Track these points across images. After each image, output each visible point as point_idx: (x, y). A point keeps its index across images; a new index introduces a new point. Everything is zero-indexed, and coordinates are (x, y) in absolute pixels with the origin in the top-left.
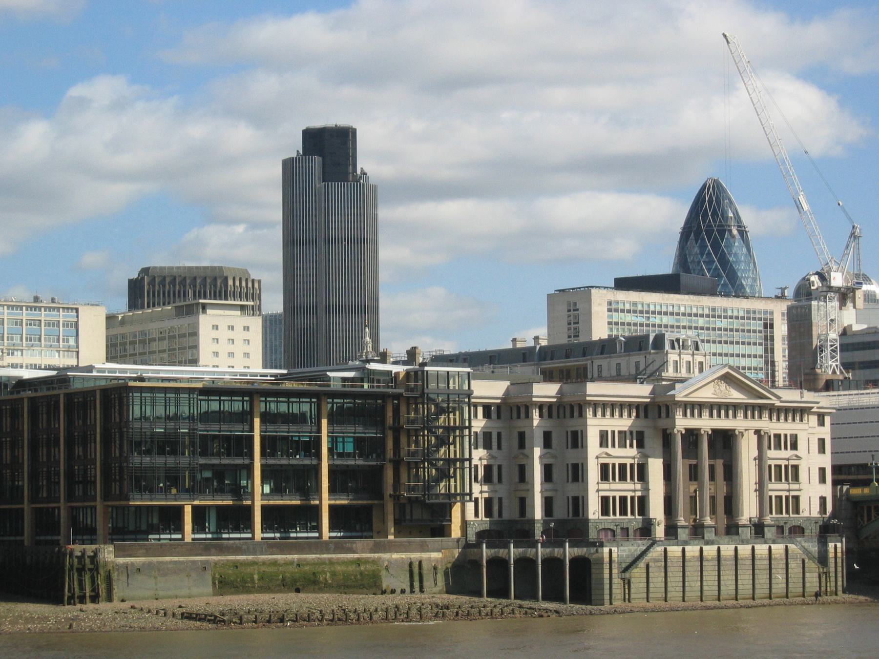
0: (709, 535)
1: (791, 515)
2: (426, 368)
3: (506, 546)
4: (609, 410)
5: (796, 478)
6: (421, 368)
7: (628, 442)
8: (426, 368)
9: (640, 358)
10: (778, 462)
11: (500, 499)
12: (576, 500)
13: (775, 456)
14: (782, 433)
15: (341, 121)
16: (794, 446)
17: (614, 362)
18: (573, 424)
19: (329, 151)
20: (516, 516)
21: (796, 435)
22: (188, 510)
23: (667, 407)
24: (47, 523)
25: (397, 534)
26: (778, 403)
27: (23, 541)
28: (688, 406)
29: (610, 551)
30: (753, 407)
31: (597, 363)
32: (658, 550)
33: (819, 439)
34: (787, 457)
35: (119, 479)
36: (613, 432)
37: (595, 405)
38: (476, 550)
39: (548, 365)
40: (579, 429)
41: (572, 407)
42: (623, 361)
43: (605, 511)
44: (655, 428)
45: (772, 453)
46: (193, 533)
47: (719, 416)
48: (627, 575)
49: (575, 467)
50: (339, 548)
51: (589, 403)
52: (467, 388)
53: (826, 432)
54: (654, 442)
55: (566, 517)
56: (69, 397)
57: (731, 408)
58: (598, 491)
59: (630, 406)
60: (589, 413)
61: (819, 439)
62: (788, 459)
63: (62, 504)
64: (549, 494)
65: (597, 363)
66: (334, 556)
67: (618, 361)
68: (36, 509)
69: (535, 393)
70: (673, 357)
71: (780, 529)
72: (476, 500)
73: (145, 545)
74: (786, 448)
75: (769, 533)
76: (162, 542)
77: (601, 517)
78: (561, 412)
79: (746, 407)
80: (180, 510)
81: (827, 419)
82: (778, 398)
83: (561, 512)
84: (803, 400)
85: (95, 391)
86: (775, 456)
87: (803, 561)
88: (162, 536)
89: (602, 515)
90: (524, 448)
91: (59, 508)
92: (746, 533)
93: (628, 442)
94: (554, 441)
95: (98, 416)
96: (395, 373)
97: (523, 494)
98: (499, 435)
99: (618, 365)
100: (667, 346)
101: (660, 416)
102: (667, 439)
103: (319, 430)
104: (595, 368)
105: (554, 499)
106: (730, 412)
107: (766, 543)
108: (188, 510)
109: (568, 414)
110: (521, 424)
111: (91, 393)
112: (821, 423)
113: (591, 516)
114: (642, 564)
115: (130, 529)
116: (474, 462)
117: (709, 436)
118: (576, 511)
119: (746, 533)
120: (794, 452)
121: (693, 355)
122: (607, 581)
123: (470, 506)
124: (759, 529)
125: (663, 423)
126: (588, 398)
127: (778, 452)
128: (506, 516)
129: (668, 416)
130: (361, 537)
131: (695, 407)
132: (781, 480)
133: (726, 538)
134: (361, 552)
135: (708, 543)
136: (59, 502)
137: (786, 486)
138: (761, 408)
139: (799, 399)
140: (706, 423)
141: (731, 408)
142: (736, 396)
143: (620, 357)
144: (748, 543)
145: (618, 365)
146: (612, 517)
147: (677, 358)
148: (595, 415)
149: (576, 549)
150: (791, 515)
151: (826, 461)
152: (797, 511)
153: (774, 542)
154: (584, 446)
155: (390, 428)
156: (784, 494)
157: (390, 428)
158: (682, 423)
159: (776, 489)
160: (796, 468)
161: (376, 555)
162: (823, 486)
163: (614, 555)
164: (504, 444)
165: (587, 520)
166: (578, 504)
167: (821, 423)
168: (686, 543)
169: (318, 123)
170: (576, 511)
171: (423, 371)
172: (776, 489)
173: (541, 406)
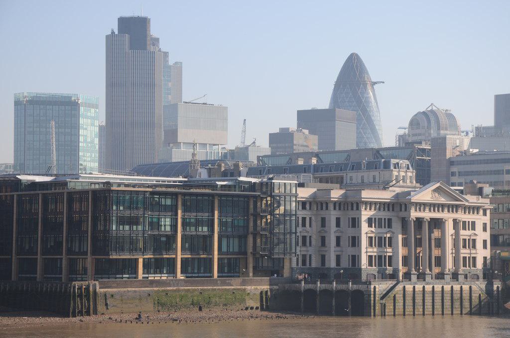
0: (428, 278)
1: (388, 267)
2: (273, 181)
3: (315, 283)
4: (368, 206)
5: (474, 247)
6: (270, 181)
7: (373, 224)
8: (273, 181)
9: (376, 173)
10: (464, 237)
11: (310, 255)
12: (354, 257)
13: (464, 234)
14: (467, 220)
15: (142, 14)
16: (474, 228)
17: (360, 174)
18: (352, 214)
19: (133, 33)
20: (319, 265)
21: (486, 223)
22: (141, 261)
23: (406, 205)
24: (52, 267)
25: (255, 275)
26: (467, 204)
27: (36, 277)
28: (450, 206)
29: (375, 287)
30: (453, 206)
31: (350, 175)
32: (400, 287)
33: (483, 223)
34: (469, 234)
35: (103, 243)
36: (469, 222)
37: (366, 203)
38: (297, 285)
39: (318, 175)
40: (356, 217)
41: (352, 204)
42: (365, 174)
43: (370, 264)
44: (398, 217)
45: (462, 232)
46: (143, 274)
47: (434, 211)
48: (384, 301)
49: (354, 238)
50: (224, 284)
51: (363, 202)
52: (283, 192)
53: (487, 219)
54: (397, 225)
55: (348, 267)
56: (71, 194)
57: (441, 207)
58: (367, 252)
59: (376, 203)
60: (363, 208)
61: (483, 223)
62: (470, 236)
63: (64, 256)
64: (338, 253)
65: (350, 175)
66: (220, 287)
67: (363, 174)
68: (70, 259)
69: (332, 196)
70: (395, 173)
71: (466, 277)
72: (298, 255)
73: (116, 281)
74: (469, 230)
75: (461, 278)
76: (124, 279)
77: (368, 267)
78: (346, 206)
79: (449, 206)
80: (136, 260)
81: (488, 212)
82: (467, 201)
83: (345, 263)
84: (479, 202)
85: (88, 191)
86: (464, 234)
87: (480, 295)
88: (124, 276)
89: (302, 265)
90: (325, 227)
91: (61, 259)
92: (448, 278)
93: (373, 224)
94: (342, 223)
95: (90, 206)
96: (254, 183)
97: (324, 253)
98: (310, 219)
99: (362, 177)
100: (392, 168)
101: (401, 210)
102: (404, 222)
103: (213, 215)
104: (349, 178)
105: (341, 256)
106: (422, 208)
107: (459, 284)
108: (141, 261)
109: (350, 208)
110: (323, 213)
111: (86, 192)
112: (485, 214)
113: (363, 267)
114: (391, 295)
115: (109, 269)
116: (298, 234)
117: (429, 223)
118: (354, 263)
119: (448, 278)
120: (473, 232)
121: (406, 172)
122: (372, 302)
123: (294, 259)
124: (455, 276)
125: (403, 214)
126: (363, 200)
127: (464, 231)
128: (314, 265)
129: (406, 210)
130: (233, 277)
131: (422, 206)
132: (466, 248)
133: (437, 281)
134: (235, 284)
135: (427, 284)
136: (87, 255)
137: (468, 251)
138: (457, 206)
139: (475, 201)
140: (427, 215)
141: (441, 207)
142: (442, 200)
143: (364, 172)
144: (449, 284)
145: (362, 177)
146: (374, 267)
147: (397, 174)
148: (366, 209)
149: (355, 286)
150: (472, 268)
151: (487, 236)
152: (474, 266)
153: (464, 284)
154: (359, 227)
155: (252, 215)
156: (467, 256)
157: (252, 215)
158: (414, 214)
159: (464, 252)
160: (474, 241)
161: (243, 287)
162: (485, 250)
163: (377, 290)
164: (313, 223)
165: (360, 269)
166: (355, 259)
167: (485, 214)
168: (416, 283)
169: (128, 14)
170: (354, 263)
171: (271, 183)
172: (464, 252)
173: (335, 203)
